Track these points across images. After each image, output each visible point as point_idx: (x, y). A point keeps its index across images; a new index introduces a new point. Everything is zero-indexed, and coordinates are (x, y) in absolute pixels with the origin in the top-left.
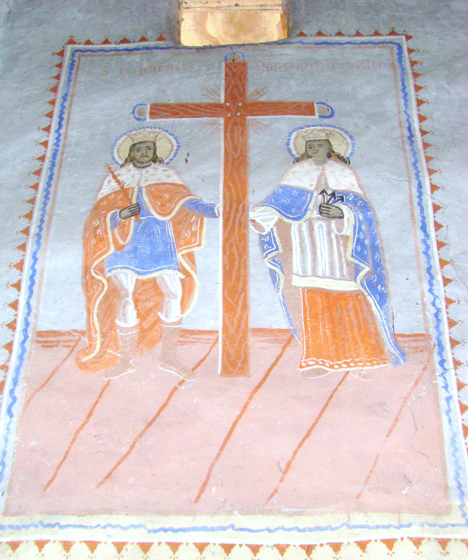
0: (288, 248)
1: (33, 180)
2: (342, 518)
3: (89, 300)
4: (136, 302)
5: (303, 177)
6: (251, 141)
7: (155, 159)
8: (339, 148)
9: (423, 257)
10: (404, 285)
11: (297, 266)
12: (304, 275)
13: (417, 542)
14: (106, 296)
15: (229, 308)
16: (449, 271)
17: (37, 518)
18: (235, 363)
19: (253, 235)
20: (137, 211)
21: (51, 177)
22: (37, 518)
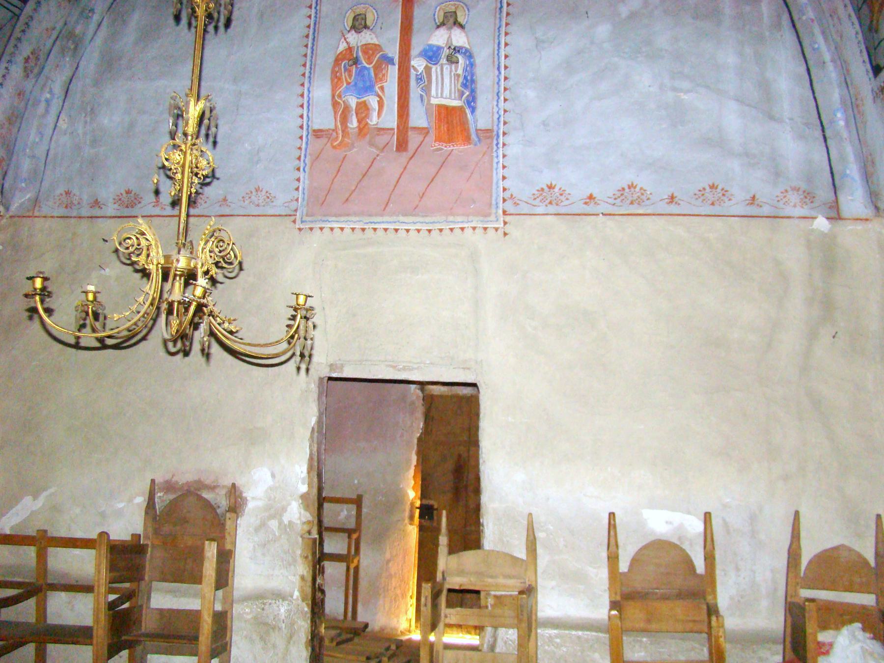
0: (430, 81)
1: (305, 42)
2: (444, 218)
3: (335, 113)
4: (357, 114)
5: (439, 38)
6: (415, 13)
7: (366, 27)
8: (460, 19)
9: (496, 86)
10: (484, 101)
11: (433, 92)
12: (437, 97)
13: (474, 228)
14: (343, 112)
15: (400, 116)
16: (508, 94)
17: (320, 218)
18: (402, 145)
19: (413, 73)
20: (356, 61)
21: (314, 39)
22: (320, 218)
